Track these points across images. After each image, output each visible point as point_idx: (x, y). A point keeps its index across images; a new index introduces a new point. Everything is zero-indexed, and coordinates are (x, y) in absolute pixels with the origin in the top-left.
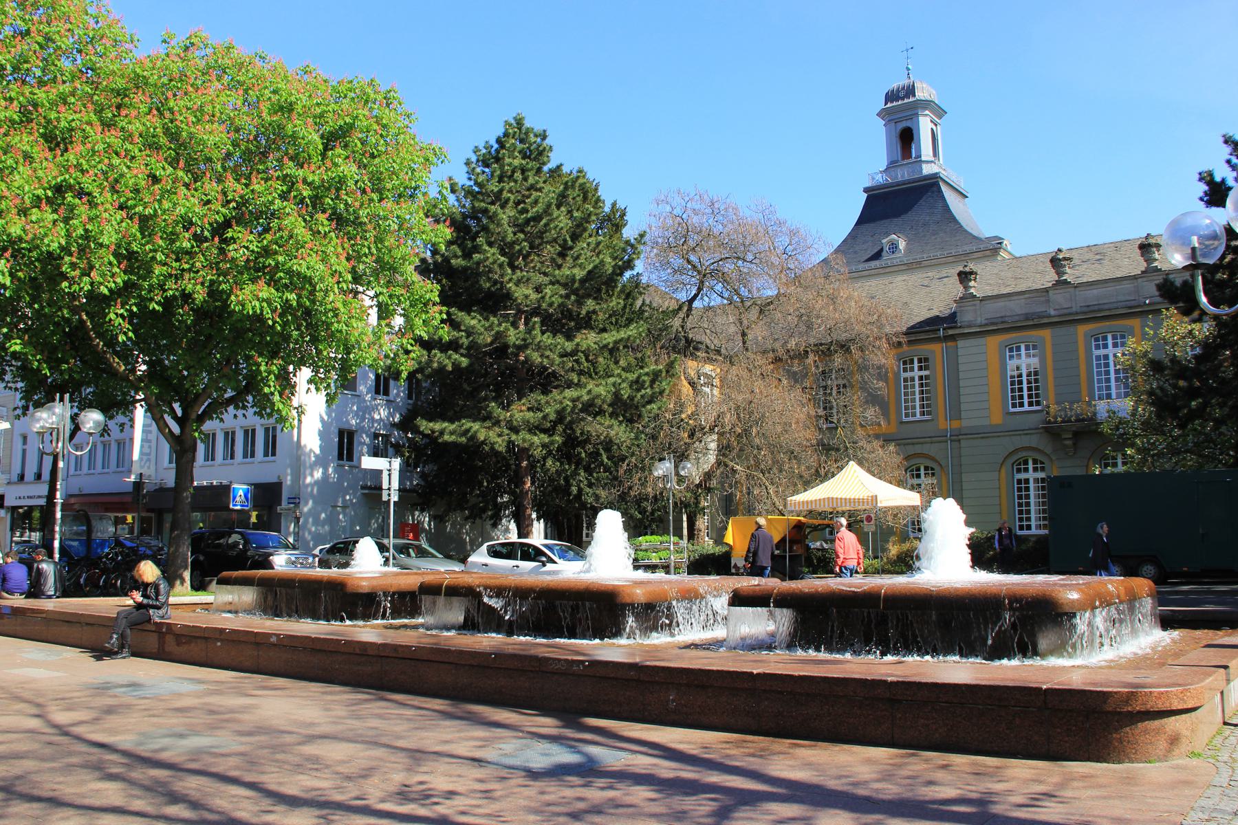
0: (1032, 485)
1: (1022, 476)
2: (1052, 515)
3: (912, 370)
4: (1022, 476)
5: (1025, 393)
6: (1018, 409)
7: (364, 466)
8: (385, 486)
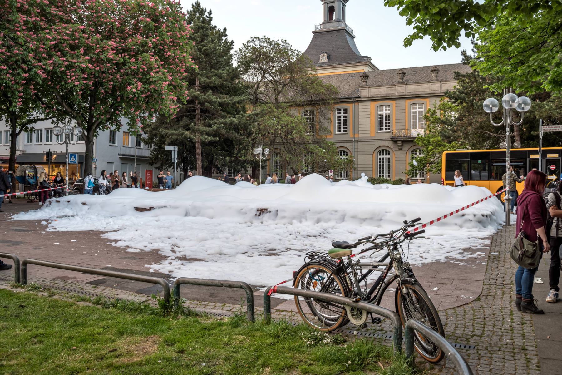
0: (385, 160)
1: (381, 156)
2: (168, 151)
3: (340, 113)
4: (381, 156)
5: (384, 122)
6: (381, 131)
7: (166, 149)
8: (173, 157)
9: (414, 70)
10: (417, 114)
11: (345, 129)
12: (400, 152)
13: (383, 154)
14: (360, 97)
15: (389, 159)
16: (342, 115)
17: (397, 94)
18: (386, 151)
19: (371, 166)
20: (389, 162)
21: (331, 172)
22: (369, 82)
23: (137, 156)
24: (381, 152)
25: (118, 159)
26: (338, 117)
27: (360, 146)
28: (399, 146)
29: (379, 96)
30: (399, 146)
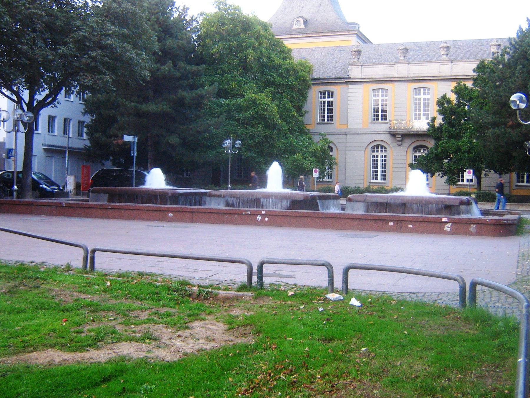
0: (379, 159)
3: (324, 97)
9: (420, 47)
10: (422, 101)
11: (330, 118)
12: (399, 148)
13: (377, 151)
14: (350, 78)
15: (385, 157)
16: (326, 100)
17: (396, 76)
18: (382, 147)
19: (362, 165)
20: (385, 160)
21: (316, 171)
22: (362, 58)
23: (69, 148)
24: (375, 148)
25: (42, 151)
26: (321, 102)
27: (348, 140)
28: (398, 141)
29: (374, 77)
30: (398, 141)
